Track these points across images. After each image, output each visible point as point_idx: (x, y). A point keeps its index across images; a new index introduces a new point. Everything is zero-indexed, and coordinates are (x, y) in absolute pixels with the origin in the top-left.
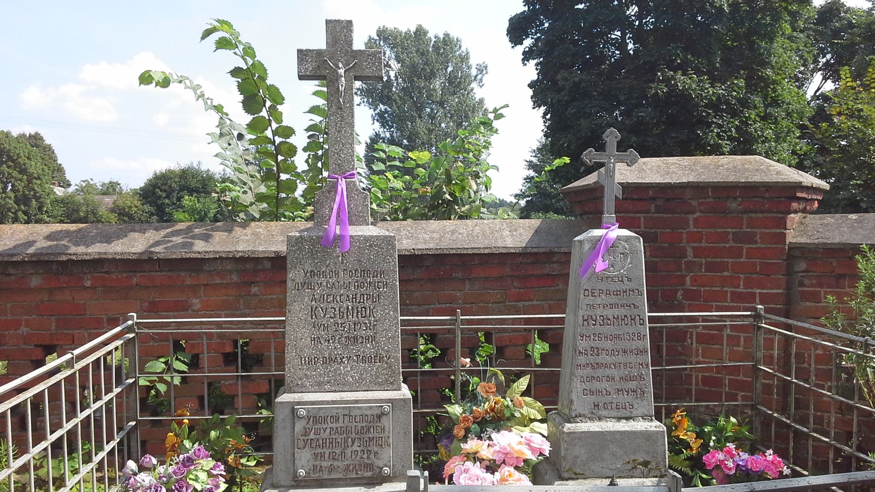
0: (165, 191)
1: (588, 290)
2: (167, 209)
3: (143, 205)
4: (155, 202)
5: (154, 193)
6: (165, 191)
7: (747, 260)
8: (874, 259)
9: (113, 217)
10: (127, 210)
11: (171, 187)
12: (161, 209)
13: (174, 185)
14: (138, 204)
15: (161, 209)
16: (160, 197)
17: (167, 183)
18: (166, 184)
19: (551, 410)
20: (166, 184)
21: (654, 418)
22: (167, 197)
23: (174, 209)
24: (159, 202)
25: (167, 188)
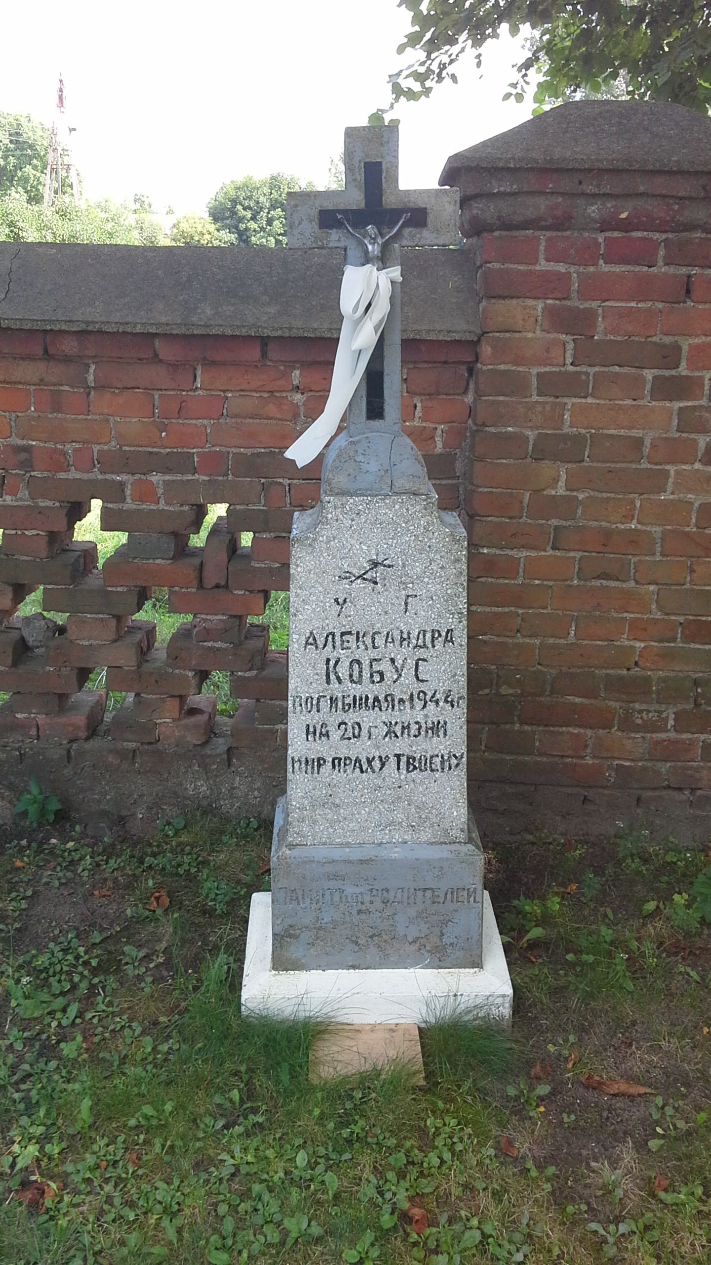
0: (250, 208)
1: (345, 724)
2: (253, 238)
3: (218, 230)
4: (237, 227)
5: (234, 213)
6: (250, 208)
7: (693, 436)
8: (0, 141)
9: (474, 240)
10: (196, 238)
11: (258, 203)
12: (245, 237)
13: (262, 199)
14: (212, 228)
15: (245, 237)
16: (241, 219)
17: (252, 196)
18: (250, 198)
19: (163, 1149)
20: (250, 198)
21: (380, 241)
22: (254, 218)
23: (263, 237)
24: (242, 226)
25: (252, 204)
